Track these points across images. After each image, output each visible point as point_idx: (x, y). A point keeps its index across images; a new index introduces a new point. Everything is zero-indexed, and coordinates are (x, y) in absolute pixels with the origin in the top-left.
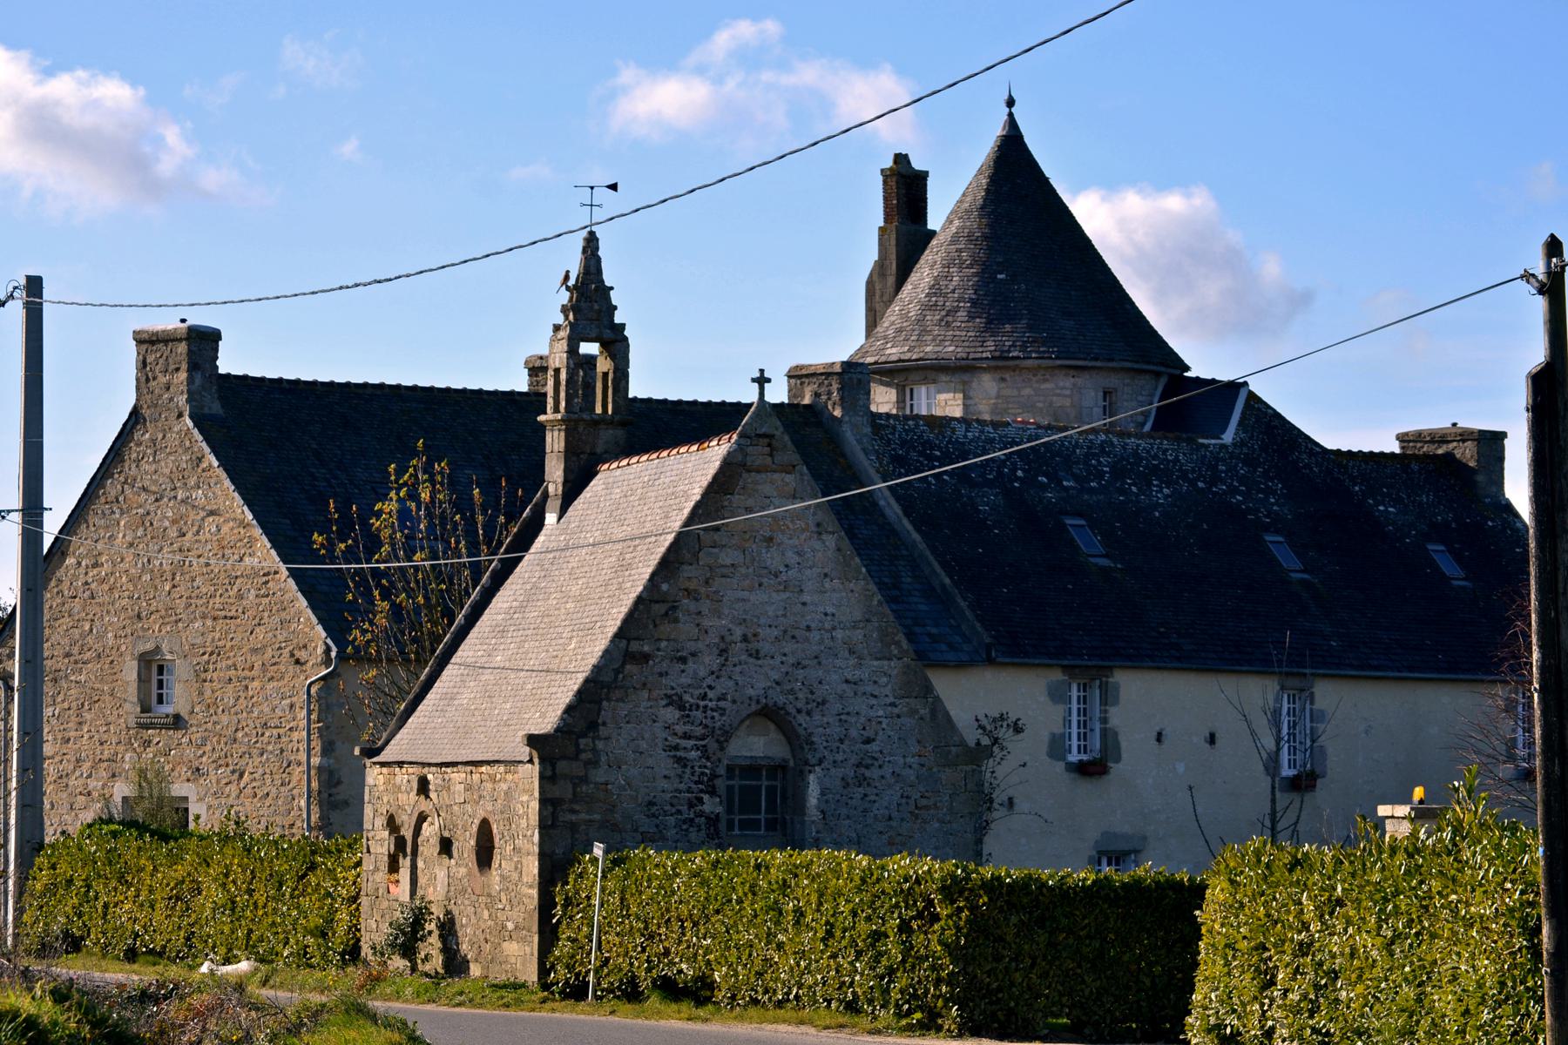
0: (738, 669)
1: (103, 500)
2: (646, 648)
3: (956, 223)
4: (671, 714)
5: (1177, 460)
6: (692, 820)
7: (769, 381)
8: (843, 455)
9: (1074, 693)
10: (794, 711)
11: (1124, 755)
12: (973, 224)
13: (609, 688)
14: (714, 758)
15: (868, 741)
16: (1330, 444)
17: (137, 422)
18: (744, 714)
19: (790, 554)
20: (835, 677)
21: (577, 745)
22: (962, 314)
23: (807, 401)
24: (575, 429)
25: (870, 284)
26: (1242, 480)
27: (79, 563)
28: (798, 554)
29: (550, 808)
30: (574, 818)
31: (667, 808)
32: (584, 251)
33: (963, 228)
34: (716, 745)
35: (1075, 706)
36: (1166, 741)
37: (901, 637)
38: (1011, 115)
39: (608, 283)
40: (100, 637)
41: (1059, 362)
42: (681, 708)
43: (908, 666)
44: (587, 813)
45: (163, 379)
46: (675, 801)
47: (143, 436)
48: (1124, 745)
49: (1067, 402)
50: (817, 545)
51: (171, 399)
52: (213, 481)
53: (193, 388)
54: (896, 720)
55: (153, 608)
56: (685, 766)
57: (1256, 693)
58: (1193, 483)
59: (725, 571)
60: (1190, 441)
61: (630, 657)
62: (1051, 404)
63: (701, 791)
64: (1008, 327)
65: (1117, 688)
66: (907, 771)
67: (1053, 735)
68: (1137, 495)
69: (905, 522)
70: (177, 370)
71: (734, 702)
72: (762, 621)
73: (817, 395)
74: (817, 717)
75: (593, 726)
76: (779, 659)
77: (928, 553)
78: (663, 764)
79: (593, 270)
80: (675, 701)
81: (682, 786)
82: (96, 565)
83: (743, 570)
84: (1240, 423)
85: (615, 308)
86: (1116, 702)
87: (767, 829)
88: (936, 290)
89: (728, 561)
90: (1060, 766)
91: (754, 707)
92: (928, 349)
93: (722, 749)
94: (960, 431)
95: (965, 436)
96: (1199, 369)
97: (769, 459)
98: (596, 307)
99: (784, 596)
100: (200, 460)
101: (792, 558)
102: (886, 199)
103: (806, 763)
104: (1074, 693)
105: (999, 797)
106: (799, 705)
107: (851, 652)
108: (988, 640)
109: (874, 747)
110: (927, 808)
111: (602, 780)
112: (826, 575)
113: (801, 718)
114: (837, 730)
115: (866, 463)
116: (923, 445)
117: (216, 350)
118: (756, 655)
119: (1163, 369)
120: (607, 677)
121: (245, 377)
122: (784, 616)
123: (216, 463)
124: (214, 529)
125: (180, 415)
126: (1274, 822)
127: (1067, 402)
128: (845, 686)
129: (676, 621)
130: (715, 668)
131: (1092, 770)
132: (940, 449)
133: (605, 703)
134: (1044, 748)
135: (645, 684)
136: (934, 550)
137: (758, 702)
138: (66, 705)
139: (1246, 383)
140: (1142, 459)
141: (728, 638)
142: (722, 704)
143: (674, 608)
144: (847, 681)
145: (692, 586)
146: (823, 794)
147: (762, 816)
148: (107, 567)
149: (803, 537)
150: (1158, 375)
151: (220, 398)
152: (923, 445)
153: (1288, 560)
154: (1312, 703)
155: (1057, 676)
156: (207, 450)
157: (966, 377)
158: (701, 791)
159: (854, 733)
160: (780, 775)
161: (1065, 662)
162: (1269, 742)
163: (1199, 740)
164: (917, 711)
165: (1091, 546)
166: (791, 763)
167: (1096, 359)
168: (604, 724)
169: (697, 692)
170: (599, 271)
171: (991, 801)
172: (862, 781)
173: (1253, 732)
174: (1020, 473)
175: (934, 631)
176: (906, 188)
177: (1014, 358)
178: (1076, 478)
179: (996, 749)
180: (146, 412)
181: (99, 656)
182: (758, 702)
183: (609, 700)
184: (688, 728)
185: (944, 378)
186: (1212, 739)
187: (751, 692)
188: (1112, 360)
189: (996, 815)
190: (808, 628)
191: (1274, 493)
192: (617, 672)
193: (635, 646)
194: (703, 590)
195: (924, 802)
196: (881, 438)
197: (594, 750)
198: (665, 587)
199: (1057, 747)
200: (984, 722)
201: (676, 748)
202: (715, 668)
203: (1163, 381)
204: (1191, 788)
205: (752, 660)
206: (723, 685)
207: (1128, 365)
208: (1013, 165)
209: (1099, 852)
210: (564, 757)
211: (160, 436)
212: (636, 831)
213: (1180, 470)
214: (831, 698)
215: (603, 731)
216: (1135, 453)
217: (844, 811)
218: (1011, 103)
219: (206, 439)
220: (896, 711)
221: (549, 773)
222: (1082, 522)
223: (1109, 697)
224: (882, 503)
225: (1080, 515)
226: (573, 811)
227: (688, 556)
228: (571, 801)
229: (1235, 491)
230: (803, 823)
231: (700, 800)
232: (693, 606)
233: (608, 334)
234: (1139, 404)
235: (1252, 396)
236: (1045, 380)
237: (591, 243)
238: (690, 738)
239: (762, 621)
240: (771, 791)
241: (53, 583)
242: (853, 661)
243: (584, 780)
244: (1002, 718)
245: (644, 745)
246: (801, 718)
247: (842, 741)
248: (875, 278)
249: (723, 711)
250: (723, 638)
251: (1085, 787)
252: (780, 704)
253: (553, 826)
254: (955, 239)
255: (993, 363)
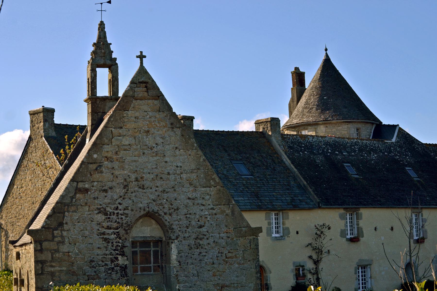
0: (134, 194)
1: (23, 166)
2: (87, 186)
3: (312, 84)
4: (100, 217)
5: (378, 146)
6: (113, 268)
7: (145, 57)
8: (272, 146)
9: (348, 217)
10: (163, 214)
11: (365, 235)
12: (317, 84)
13: (68, 206)
14: (123, 238)
15: (201, 227)
16: (424, 142)
17: (31, 141)
18: (138, 216)
19: (158, 138)
20: (183, 197)
21: (53, 234)
22: (314, 109)
23: (261, 131)
24: (96, 102)
25: (290, 105)
26: (398, 152)
27: (17, 187)
28: (162, 138)
29: (40, 265)
30: (52, 269)
31: (100, 263)
32: (99, 29)
33: (314, 85)
34: (124, 232)
35: (348, 221)
36: (378, 230)
37: (215, 176)
38: (326, 53)
39: (109, 42)
40: (24, 211)
41: (343, 121)
42: (106, 214)
43: (220, 190)
44: (59, 267)
45: (37, 126)
46: (104, 260)
47: (32, 145)
48: (364, 232)
49: (346, 132)
50: (172, 134)
51: (39, 132)
52: (51, 157)
53: (45, 128)
54: (214, 216)
55: (37, 200)
56: (109, 242)
57: (404, 214)
58: (383, 153)
59: (126, 147)
60: (382, 141)
61: (78, 190)
62: (341, 133)
63: (117, 254)
64: (328, 112)
65: (361, 214)
66: (221, 241)
67: (342, 230)
68: (366, 157)
69: (292, 165)
70: (41, 122)
71: (132, 210)
72: (145, 171)
73: (264, 128)
74: (174, 216)
75: (61, 224)
76: (154, 190)
77: (299, 175)
78: (98, 242)
79: (102, 36)
80: (102, 211)
81: (108, 252)
82: (22, 187)
83: (135, 147)
84: (397, 136)
85: (112, 52)
86: (361, 219)
87: (154, 271)
88: (307, 103)
89: (127, 143)
90: (344, 239)
91: (142, 213)
92: (305, 119)
93: (127, 233)
94: (311, 139)
95: (312, 140)
96: (385, 121)
97: (146, 93)
98: (103, 51)
99: (155, 158)
100: (47, 150)
101: (160, 141)
102: (293, 80)
103: (170, 238)
104: (348, 217)
105: (324, 250)
106: (165, 211)
107: (191, 184)
108: (318, 201)
109: (204, 229)
110: (230, 257)
111: (67, 251)
112: (176, 148)
113: (167, 217)
114: (185, 222)
115: (279, 148)
116: (299, 143)
117: (53, 115)
118: (143, 187)
119: (374, 122)
120: (67, 201)
121: (67, 125)
122: (156, 168)
123: (51, 151)
124: (52, 173)
125: (42, 137)
126: (410, 253)
127: (346, 132)
128: (188, 201)
129: (102, 172)
130: (122, 194)
131: (354, 240)
132: (304, 144)
133: (66, 213)
134: (339, 234)
135: (86, 204)
136: (301, 174)
137: (144, 210)
138: (16, 233)
139: (398, 125)
140: (368, 147)
141: (128, 180)
142: (126, 212)
143: (100, 166)
144: (189, 198)
145: (109, 155)
146: (179, 253)
147: (152, 265)
148: (24, 188)
149: (164, 130)
150: (373, 124)
151: (55, 131)
152: (299, 143)
153: (413, 174)
154: (422, 216)
155: (342, 211)
156: (49, 147)
157: (316, 127)
158: (117, 254)
159: (193, 223)
160: (160, 244)
161: (344, 207)
162: (408, 229)
163: (388, 229)
164: (225, 211)
165: (352, 172)
166: (164, 239)
167: (354, 119)
168: (66, 223)
169: (113, 207)
170: (105, 37)
171: (322, 251)
172: (198, 246)
173: (402, 224)
174: (330, 151)
175: (301, 198)
176: (299, 77)
177: (329, 120)
178: (347, 152)
179: (322, 235)
180: (33, 137)
181: (23, 217)
182: (144, 210)
183: (68, 211)
184: (109, 224)
185: (309, 127)
186: (392, 229)
187: (141, 205)
188: (359, 119)
189: (323, 256)
190: (169, 174)
191: (408, 155)
192: (72, 198)
193: (81, 185)
194: (115, 157)
195: (230, 255)
196: (285, 141)
197: (62, 236)
198: (95, 156)
199: (343, 234)
200: (318, 227)
201: (104, 234)
202: (122, 194)
203: (374, 126)
204: (383, 244)
205: (140, 190)
206: (127, 203)
207: (364, 121)
208: (328, 67)
209: (358, 266)
210: (46, 240)
211: (37, 144)
212: (85, 274)
213: (380, 149)
214: (181, 207)
215: (66, 227)
216: (366, 145)
217: (190, 261)
218: (326, 50)
219: (48, 144)
220: (214, 212)
221: (39, 248)
222: (350, 165)
223: (359, 217)
224: (284, 160)
225: (349, 163)
226: (52, 266)
227: (106, 141)
228: (51, 262)
229: (397, 155)
230: (170, 267)
231: (117, 259)
232: (109, 165)
233: (109, 62)
234: (367, 131)
235: (400, 129)
236: (339, 126)
237: (102, 25)
238: (110, 229)
239: (145, 171)
240: (156, 253)
241: (11, 194)
242: (191, 189)
243: (57, 251)
244: (324, 225)
245: (87, 233)
246: (167, 217)
247: (187, 227)
248: (291, 103)
249: (127, 215)
250: (125, 180)
251: (353, 246)
252: (156, 210)
253: (42, 274)
254: (312, 89)
255: (324, 122)
